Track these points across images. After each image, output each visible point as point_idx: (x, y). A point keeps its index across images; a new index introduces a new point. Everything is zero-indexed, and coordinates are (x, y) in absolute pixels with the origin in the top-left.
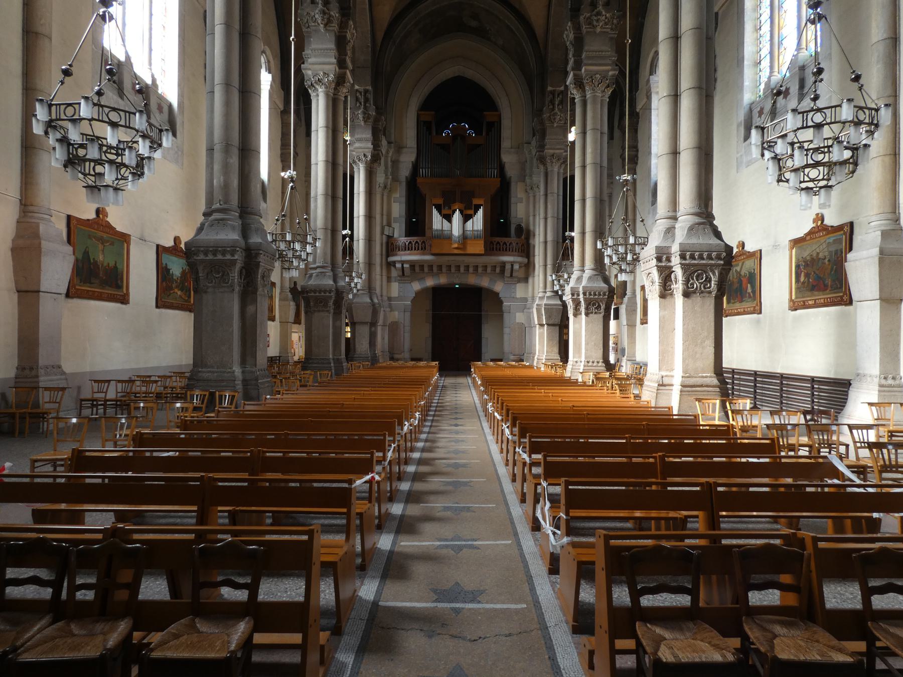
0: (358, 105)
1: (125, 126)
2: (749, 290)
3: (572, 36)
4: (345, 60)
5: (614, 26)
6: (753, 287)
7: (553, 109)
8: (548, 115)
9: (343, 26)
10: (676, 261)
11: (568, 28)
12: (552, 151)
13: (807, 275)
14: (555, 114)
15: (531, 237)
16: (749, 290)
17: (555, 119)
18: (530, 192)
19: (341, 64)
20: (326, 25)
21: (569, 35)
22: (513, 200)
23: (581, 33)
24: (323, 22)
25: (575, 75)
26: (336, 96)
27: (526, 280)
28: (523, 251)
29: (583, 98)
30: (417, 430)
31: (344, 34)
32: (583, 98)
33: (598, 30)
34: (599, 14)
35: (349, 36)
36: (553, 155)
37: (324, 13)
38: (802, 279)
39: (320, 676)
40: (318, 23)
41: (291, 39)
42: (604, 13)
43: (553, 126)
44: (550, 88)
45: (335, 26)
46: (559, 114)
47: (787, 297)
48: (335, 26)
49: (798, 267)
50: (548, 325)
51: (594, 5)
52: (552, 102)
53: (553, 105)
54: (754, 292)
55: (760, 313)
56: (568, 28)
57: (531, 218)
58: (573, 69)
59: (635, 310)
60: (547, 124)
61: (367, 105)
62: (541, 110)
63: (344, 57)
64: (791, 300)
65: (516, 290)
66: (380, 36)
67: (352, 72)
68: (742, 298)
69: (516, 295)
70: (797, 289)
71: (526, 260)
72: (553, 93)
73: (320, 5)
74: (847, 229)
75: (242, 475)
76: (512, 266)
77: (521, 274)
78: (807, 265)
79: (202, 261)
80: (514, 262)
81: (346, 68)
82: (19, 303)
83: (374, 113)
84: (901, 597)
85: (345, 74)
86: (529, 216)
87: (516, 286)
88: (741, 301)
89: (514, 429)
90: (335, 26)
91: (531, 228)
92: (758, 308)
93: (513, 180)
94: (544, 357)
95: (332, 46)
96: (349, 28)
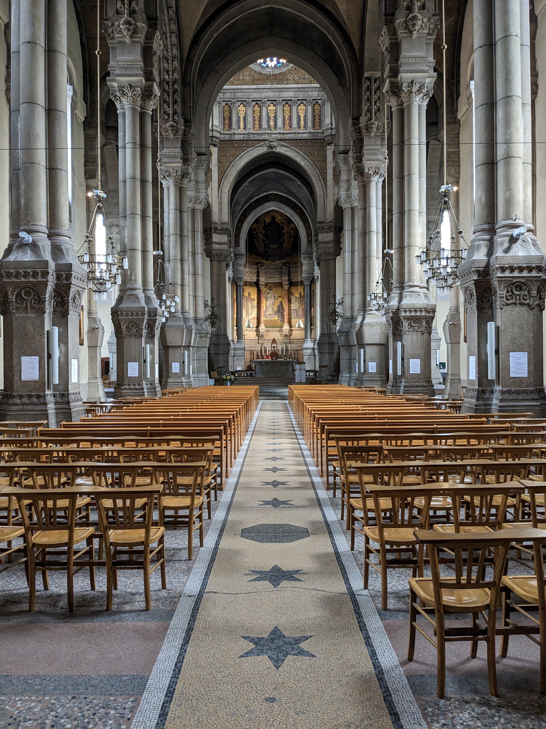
0: (166, 117)
1: (115, 279)
3: (387, 42)
4: (151, 73)
5: (431, 31)
8: (403, 19)
9: (149, 37)
11: (383, 33)
14: (414, 18)
17: (414, 25)
19: (148, 76)
20: (131, 37)
21: (385, 41)
23: (397, 39)
24: (129, 33)
25: (391, 83)
26: (143, 110)
29: (399, 107)
30: (313, 424)
31: (150, 45)
32: (399, 107)
33: (373, 135)
35: (155, 46)
36: (412, 82)
37: (127, 23)
40: (123, 35)
41: (96, 53)
44: (366, 75)
45: (141, 37)
48: (140, 37)
51: (410, 9)
56: (383, 33)
58: (389, 77)
61: (176, 117)
62: (358, 119)
63: (150, 68)
66: (187, 43)
67: (160, 85)
72: (369, 79)
73: (126, 15)
75: (492, 368)
79: (11, 284)
81: (154, 80)
83: (182, 127)
84: (544, 531)
85: (152, 86)
87: (311, 489)
89: (323, 435)
90: (140, 37)
95: (179, 150)
96: (156, 38)
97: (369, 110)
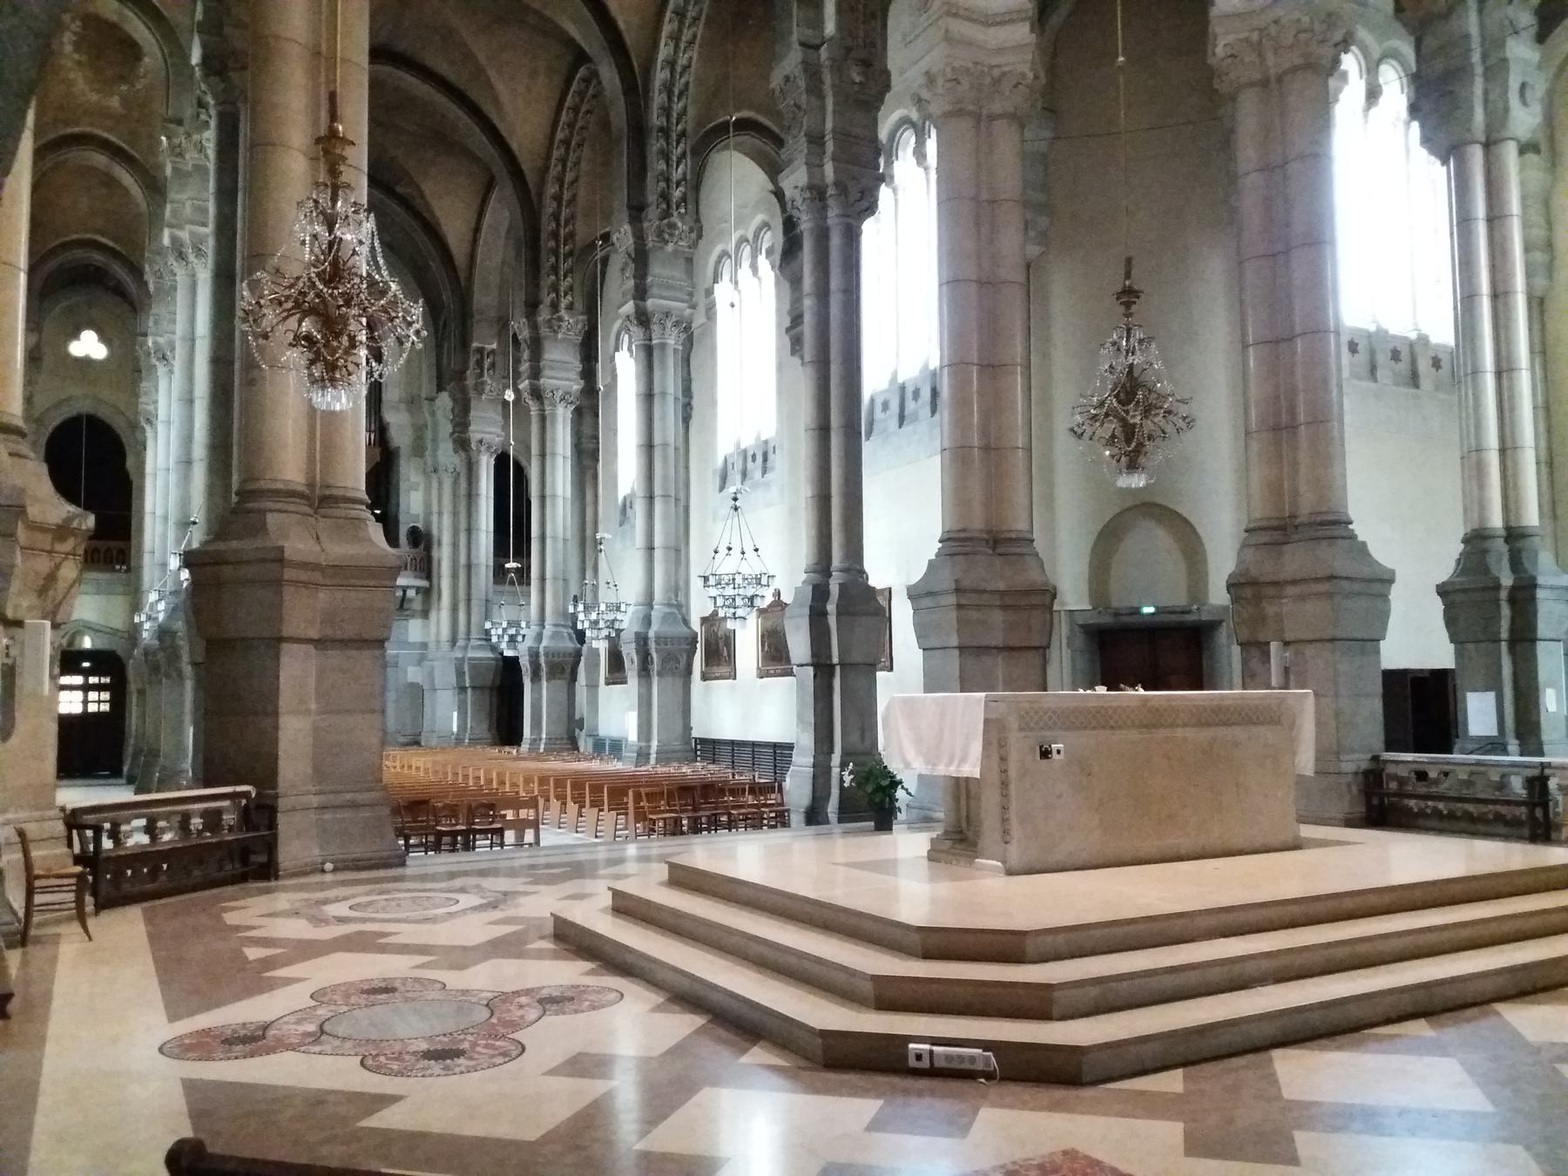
2: (725, 654)
6: (729, 651)
7: (481, 375)
10: (466, 669)
12: (479, 436)
13: (769, 646)
15: (435, 547)
16: (725, 654)
17: (671, 235)
18: (434, 475)
22: (403, 486)
27: (425, 614)
28: (422, 570)
33: (560, 336)
34: (560, 319)
38: (766, 648)
39: (1119, 2)
42: (566, 318)
43: (556, 339)
44: (475, 345)
46: (489, 382)
47: (756, 664)
49: (763, 636)
50: (473, 688)
52: (480, 363)
53: (482, 368)
54: (729, 655)
55: (735, 679)
57: (435, 518)
59: (598, 665)
60: (472, 394)
64: (758, 668)
65: (407, 631)
68: (719, 660)
69: (407, 637)
70: (763, 657)
71: (424, 583)
72: (480, 351)
74: (887, 593)
76: (405, 592)
77: (417, 605)
78: (769, 636)
80: (408, 587)
82: (925, 659)
86: (431, 513)
88: (718, 665)
91: (435, 532)
92: (733, 674)
93: (402, 452)
94: (467, 736)
97: (665, 196)
